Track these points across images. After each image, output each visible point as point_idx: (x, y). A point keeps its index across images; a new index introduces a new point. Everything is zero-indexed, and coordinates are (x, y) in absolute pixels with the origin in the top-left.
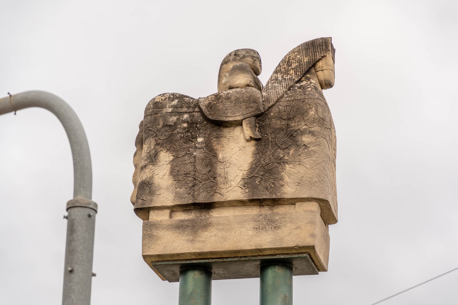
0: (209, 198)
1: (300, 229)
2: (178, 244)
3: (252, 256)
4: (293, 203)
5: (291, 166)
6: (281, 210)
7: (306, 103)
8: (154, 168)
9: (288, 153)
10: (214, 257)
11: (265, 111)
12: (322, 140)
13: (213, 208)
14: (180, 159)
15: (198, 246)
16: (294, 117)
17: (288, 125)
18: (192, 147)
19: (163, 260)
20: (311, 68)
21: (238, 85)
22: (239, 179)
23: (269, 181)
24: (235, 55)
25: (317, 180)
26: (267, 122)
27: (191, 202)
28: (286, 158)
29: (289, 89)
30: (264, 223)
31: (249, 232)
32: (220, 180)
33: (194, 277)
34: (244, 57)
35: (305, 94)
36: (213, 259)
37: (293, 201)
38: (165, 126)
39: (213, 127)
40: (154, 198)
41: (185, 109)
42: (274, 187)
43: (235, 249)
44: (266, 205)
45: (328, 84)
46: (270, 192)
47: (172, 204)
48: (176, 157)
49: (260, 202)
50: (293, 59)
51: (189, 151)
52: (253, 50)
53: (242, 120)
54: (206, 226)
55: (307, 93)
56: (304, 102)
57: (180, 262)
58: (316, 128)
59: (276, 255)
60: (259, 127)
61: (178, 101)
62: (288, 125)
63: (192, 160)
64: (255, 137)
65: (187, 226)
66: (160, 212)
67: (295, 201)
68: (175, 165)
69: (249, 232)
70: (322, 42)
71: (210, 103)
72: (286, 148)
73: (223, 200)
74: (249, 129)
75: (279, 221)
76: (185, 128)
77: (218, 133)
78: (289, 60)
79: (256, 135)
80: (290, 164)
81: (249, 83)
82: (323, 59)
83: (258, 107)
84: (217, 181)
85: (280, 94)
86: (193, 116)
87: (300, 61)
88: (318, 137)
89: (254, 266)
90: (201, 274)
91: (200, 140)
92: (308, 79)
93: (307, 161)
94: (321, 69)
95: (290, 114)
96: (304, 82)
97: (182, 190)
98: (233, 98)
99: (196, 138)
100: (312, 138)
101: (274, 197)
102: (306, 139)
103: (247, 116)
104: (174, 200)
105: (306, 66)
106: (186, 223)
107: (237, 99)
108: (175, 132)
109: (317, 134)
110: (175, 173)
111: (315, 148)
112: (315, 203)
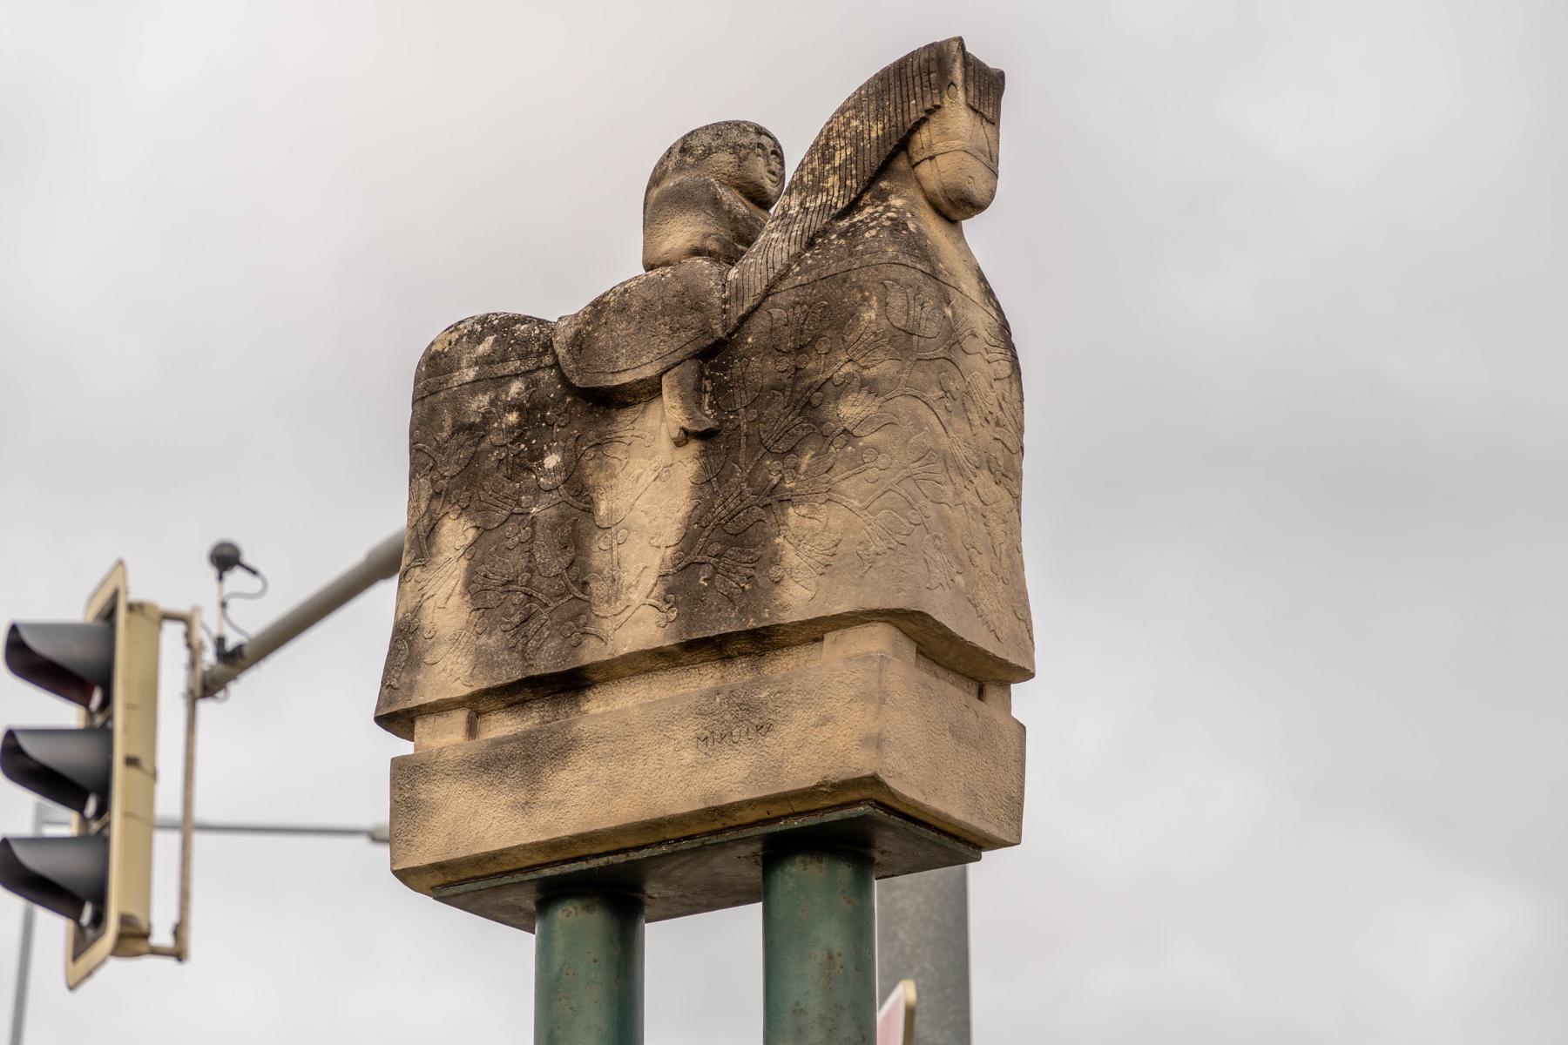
0: (568, 655)
1: (830, 725)
2: (488, 821)
3: (710, 833)
4: (817, 636)
5: (803, 512)
6: (782, 665)
7: (853, 285)
8: (425, 576)
9: (796, 468)
10: (599, 850)
11: (730, 335)
12: (901, 404)
13: (589, 687)
14: (494, 536)
15: (542, 821)
16: (815, 338)
17: (797, 369)
18: (527, 492)
19: (461, 877)
20: (891, 157)
21: (668, 257)
22: (650, 579)
23: (737, 572)
24: (683, 151)
25: (880, 546)
26: (737, 368)
27: (517, 675)
28: (789, 485)
29: (811, 244)
30: (728, 717)
31: (685, 755)
32: (598, 588)
33: (804, 877)
34: (708, 151)
35: (851, 255)
36: (598, 856)
37: (814, 631)
38: (458, 431)
39: (590, 412)
40: (420, 677)
41: (514, 365)
42: (752, 591)
43: (647, 817)
44: (740, 654)
45: (957, 206)
46: (741, 611)
47: (467, 691)
48: (483, 530)
49: (717, 648)
50: (839, 136)
51: (518, 504)
52: (737, 124)
53: (660, 376)
54: (561, 750)
55: (860, 248)
56: (845, 281)
57: (533, 876)
58: (883, 367)
59: (778, 819)
60: (712, 393)
61: (496, 341)
62: (797, 369)
63: (525, 534)
64: (695, 428)
65: (511, 758)
66: (441, 721)
67: (819, 628)
68: (478, 557)
69: (685, 755)
70: (927, 61)
71: (578, 333)
72: (790, 451)
73: (606, 658)
74: (678, 404)
75: (770, 704)
76: (511, 429)
77: (602, 429)
78: (828, 140)
79: (698, 422)
80: (801, 502)
81: (698, 244)
82: (933, 119)
83: (705, 323)
84: (590, 594)
85: (778, 267)
86: (535, 383)
87: (859, 136)
88: (888, 396)
89: (739, 864)
90: (588, 908)
91: (552, 461)
92: (883, 196)
93: (852, 488)
94: (928, 154)
95: (802, 331)
96: (869, 210)
97: (491, 642)
98: (636, 305)
99: (542, 456)
100: (868, 402)
101: (752, 624)
102: (850, 410)
103: (671, 360)
104: (471, 675)
105: (874, 154)
106: (508, 748)
107: (647, 306)
108: (485, 445)
109: (886, 385)
110: (476, 588)
111: (877, 435)
112: (880, 625)
